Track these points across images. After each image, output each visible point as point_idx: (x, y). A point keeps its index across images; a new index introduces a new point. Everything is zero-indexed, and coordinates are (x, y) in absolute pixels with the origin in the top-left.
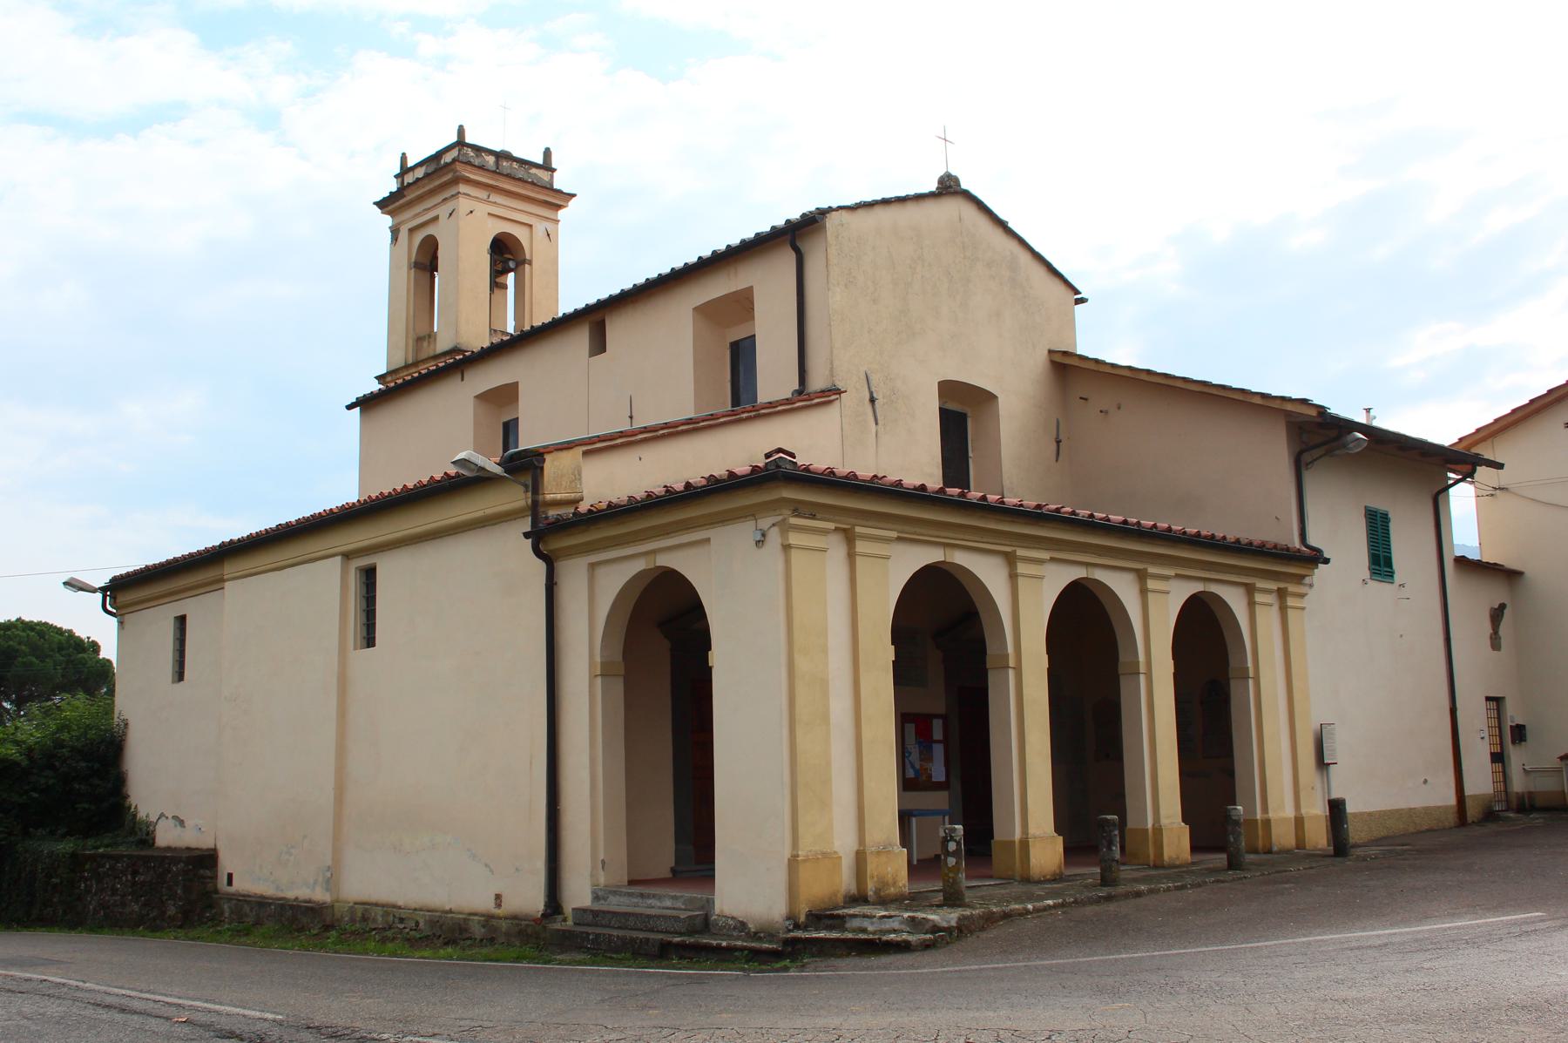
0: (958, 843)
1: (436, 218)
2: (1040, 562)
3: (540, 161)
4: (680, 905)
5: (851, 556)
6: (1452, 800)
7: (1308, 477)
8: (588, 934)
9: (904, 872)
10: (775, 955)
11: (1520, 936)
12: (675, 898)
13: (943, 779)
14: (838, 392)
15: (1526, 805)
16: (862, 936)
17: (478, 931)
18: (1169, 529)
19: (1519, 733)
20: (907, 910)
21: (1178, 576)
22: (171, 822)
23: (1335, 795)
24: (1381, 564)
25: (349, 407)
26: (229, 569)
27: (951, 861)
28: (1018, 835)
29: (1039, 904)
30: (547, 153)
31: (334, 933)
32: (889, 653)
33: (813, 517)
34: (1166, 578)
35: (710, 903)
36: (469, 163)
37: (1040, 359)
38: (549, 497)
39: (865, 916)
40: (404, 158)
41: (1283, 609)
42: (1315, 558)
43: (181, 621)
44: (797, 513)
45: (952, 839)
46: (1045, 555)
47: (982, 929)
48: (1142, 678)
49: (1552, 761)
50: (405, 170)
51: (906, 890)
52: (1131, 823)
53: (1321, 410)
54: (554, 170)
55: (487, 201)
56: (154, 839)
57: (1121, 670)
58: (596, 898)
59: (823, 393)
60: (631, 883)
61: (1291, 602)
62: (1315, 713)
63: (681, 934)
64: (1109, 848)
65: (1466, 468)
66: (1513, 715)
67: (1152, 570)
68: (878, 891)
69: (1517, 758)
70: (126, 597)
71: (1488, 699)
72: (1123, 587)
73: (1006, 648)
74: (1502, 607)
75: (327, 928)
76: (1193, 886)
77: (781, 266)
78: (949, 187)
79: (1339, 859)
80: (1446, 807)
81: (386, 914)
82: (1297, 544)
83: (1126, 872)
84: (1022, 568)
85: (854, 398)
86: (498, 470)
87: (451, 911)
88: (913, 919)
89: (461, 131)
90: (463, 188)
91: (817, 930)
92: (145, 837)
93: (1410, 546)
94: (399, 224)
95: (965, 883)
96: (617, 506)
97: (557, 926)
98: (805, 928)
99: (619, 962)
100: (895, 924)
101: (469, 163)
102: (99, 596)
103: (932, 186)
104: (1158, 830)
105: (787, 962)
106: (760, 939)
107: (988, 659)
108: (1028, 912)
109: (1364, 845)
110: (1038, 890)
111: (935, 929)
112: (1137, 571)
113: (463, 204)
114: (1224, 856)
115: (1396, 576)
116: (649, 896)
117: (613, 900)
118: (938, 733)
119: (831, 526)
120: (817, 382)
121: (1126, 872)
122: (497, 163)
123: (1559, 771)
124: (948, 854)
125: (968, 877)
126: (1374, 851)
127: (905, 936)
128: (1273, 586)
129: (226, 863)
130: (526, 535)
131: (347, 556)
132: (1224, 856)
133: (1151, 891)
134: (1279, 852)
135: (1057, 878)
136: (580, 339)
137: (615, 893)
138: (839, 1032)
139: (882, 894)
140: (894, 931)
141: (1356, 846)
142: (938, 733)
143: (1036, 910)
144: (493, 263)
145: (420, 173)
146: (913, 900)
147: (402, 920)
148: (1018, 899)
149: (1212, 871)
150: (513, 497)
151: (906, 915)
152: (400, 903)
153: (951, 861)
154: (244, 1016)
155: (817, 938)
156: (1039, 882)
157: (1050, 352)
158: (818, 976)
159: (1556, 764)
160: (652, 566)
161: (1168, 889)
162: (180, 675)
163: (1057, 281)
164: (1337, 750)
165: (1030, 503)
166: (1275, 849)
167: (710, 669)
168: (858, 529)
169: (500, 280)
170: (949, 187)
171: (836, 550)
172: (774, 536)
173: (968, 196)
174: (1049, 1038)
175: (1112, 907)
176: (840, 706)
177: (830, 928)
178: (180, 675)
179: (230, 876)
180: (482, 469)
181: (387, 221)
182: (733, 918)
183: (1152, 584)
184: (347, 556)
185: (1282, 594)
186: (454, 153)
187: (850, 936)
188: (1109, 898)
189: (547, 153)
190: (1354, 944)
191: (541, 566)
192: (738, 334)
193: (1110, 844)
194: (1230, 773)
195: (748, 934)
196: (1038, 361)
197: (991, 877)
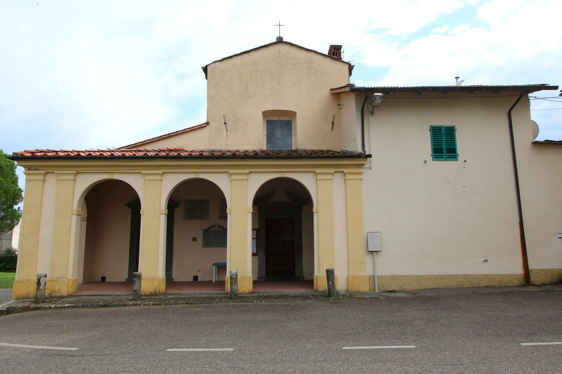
6: (520, 271)
33: (36, 170)
78: (280, 41)
139: (52, 295)
170: (280, 41)
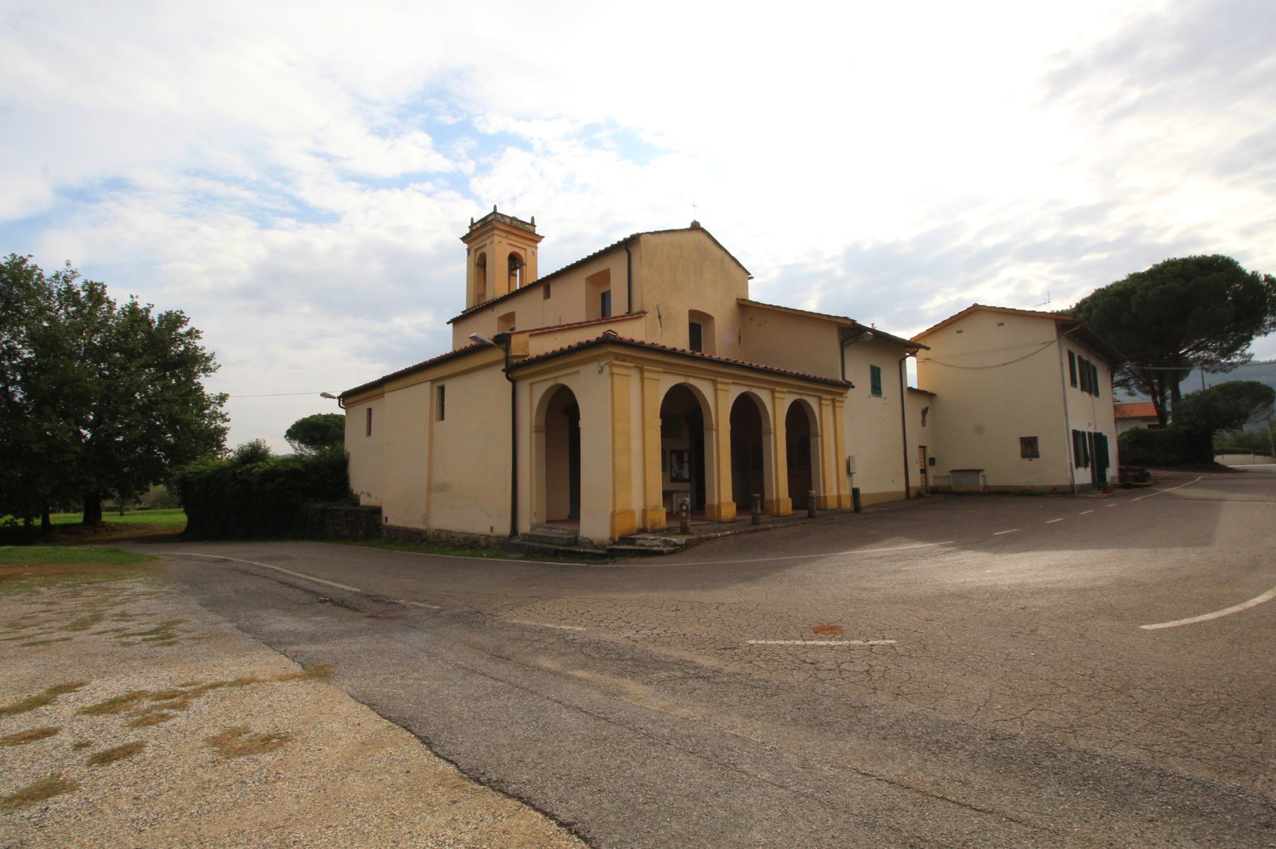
0: (687, 506)
1: (485, 245)
2: (728, 384)
3: (530, 222)
4: (565, 532)
5: (642, 379)
6: (903, 489)
7: (847, 352)
8: (525, 545)
9: (664, 518)
10: (603, 556)
11: (945, 553)
12: (564, 529)
13: (688, 477)
14: (645, 313)
15: (935, 491)
16: (643, 548)
17: (483, 543)
18: (785, 371)
19: (932, 461)
20: (663, 536)
21: (788, 392)
22: (366, 495)
23: (855, 486)
24: (876, 389)
25: (448, 323)
26: (387, 387)
27: (684, 514)
28: (716, 502)
29: (724, 534)
30: (533, 219)
31: (425, 543)
32: (659, 422)
33: (624, 361)
34: (783, 392)
35: (578, 532)
36: (498, 221)
37: (733, 301)
38: (513, 354)
39: (644, 539)
40: (472, 219)
41: (834, 407)
42: (849, 386)
43: (370, 410)
44: (617, 359)
45: (684, 504)
46: (731, 381)
47: (697, 545)
48: (772, 436)
49: (945, 473)
50: (473, 224)
51: (665, 527)
52: (767, 497)
53: (853, 322)
54: (535, 226)
55: (506, 238)
56: (359, 502)
57: (763, 431)
58: (532, 529)
59: (638, 313)
60: (548, 522)
61: (837, 404)
62: (848, 450)
63: (564, 546)
64: (756, 509)
65: (912, 351)
66: (930, 453)
67: (777, 389)
68: (652, 528)
69: (931, 471)
70: (349, 401)
71: (920, 447)
72: (764, 396)
73: (712, 421)
74: (927, 409)
75: (423, 540)
76: (793, 525)
77: (622, 258)
78: (696, 227)
79: (856, 514)
80: (902, 492)
81: (447, 535)
82: (840, 379)
83: (763, 518)
84: (719, 386)
85: (651, 316)
86: (491, 342)
87: (472, 534)
88: (665, 540)
89: (495, 207)
90: (496, 232)
91: (623, 545)
92: (356, 501)
93: (888, 382)
94: (471, 247)
95: (690, 523)
96: (540, 357)
97: (514, 541)
98: (618, 544)
99: (536, 559)
100: (657, 543)
101: (498, 221)
102: (337, 400)
103: (689, 226)
104: (778, 501)
105: (608, 560)
106: (599, 549)
107: (704, 426)
108: (718, 537)
109: (867, 507)
110: (724, 527)
111: (675, 545)
112: (770, 389)
113: (496, 239)
114: (806, 512)
115: (883, 394)
116: (554, 528)
117: (539, 529)
118: (686, 458)
119: (633, 365)
120: (636, 309)
121: (763, 518)
122: (511, 222)
123: (949, 477)
124: (682, 511)
125: (692, 520)
126: (871, 510)
127: (661, 548)
128: (830, 397)
129: (385, 513)
130: (503, 370)
131: (433, 381)
132: (806, 512)
133: (774, 528)
134: (831, 510)
135: (733, 521)
136: (540, 292)
137: (540, 527)
138: (615, 602)
140: (657, 546)
141: (863, 508)
142: (686, 458)
143: (722, 536)
144: (510, 265)
145: (478, 225)
146: (668, 531)
147: (453, 538)
148: (715, 531)
149: (801, 518)
150: (498, 354)
151: (663, 538)
152: (453, 530)
153: (684, 514)
154: (343, 589)
155: (622, 549)
156: (724, 523)
157: (737, 299)
158: (619, 568)
159: (948, 474)
160: (555, 384)
161: (781, 527)
162: (369, 433)
163: (741, 269)
164: (857, 467)
165: (723, 358)
166: (829, 509)
167: (579, 428)
168: (645, 367)
169: (514, 272)
170: (696, 227)
171: (635, 376)
172: (607, 369)
173: (703, 230)
174: (717, 608)
175: (756, 535)
176: (636, 445)
177: (629, 544)
178: (369, 433)
179: (386, 518)
180: (483, 341)
181: (466, 246)
182: (588, 539)
183: (777, 395)
184: (433, 381)
185: (833, 401)
186: (492, 217)
187: (637, 548)
188: (755, 531)
189: (533, 219)
190: (868, 556)
191: (509, 384)
192: (604, 290)
193: (756, 506)
194: (809, 476)
195: (594, 546)
196: (731, 303)
197: (704, 520)
